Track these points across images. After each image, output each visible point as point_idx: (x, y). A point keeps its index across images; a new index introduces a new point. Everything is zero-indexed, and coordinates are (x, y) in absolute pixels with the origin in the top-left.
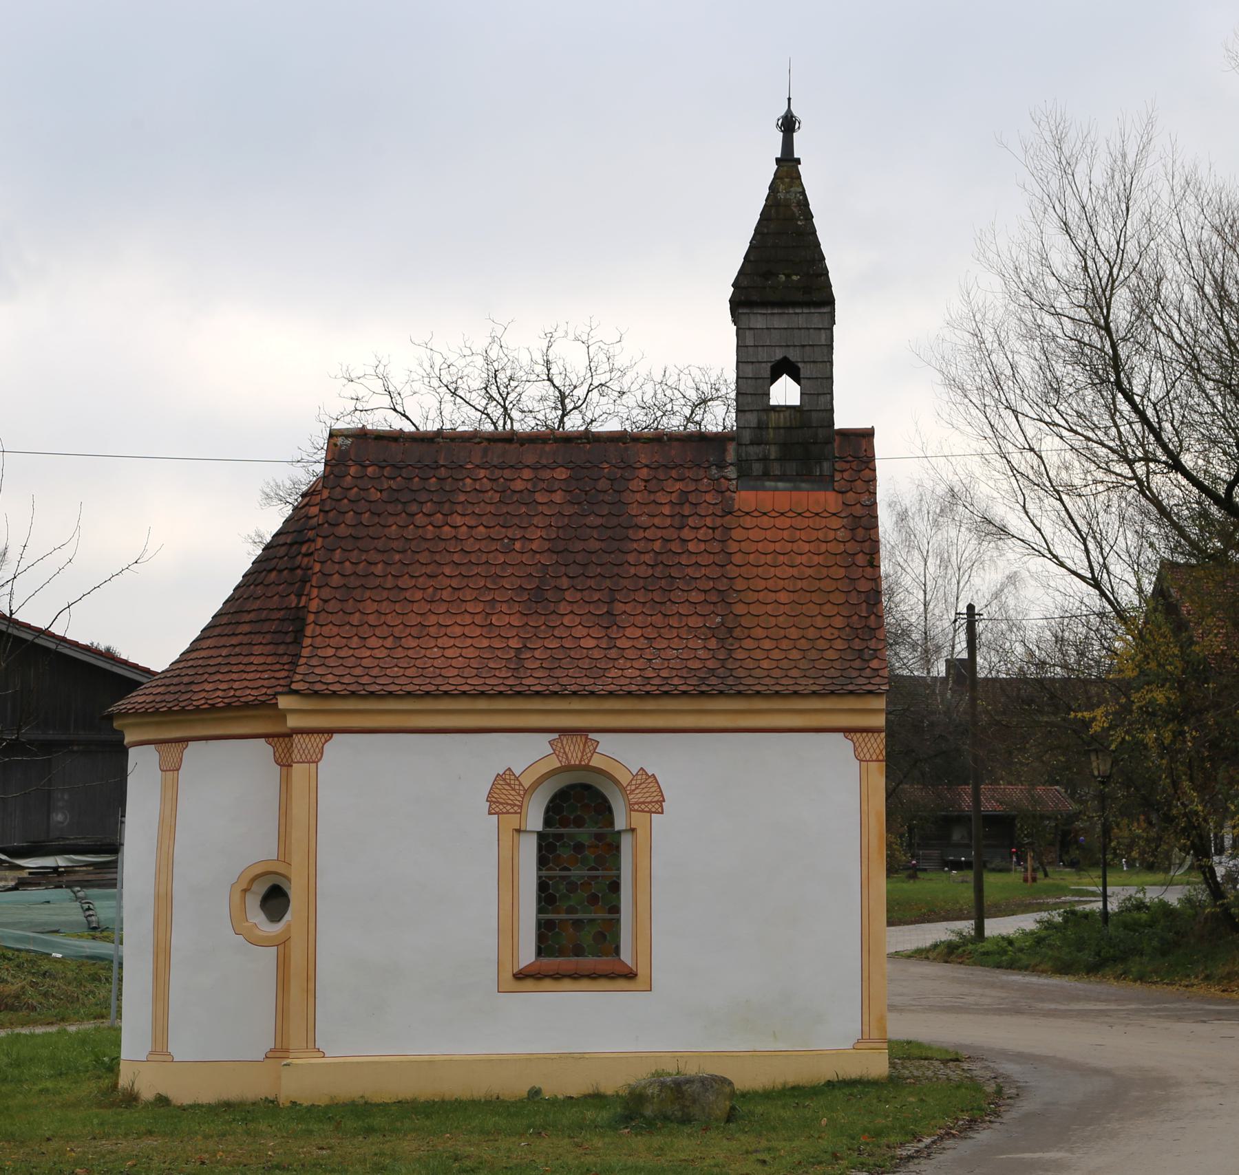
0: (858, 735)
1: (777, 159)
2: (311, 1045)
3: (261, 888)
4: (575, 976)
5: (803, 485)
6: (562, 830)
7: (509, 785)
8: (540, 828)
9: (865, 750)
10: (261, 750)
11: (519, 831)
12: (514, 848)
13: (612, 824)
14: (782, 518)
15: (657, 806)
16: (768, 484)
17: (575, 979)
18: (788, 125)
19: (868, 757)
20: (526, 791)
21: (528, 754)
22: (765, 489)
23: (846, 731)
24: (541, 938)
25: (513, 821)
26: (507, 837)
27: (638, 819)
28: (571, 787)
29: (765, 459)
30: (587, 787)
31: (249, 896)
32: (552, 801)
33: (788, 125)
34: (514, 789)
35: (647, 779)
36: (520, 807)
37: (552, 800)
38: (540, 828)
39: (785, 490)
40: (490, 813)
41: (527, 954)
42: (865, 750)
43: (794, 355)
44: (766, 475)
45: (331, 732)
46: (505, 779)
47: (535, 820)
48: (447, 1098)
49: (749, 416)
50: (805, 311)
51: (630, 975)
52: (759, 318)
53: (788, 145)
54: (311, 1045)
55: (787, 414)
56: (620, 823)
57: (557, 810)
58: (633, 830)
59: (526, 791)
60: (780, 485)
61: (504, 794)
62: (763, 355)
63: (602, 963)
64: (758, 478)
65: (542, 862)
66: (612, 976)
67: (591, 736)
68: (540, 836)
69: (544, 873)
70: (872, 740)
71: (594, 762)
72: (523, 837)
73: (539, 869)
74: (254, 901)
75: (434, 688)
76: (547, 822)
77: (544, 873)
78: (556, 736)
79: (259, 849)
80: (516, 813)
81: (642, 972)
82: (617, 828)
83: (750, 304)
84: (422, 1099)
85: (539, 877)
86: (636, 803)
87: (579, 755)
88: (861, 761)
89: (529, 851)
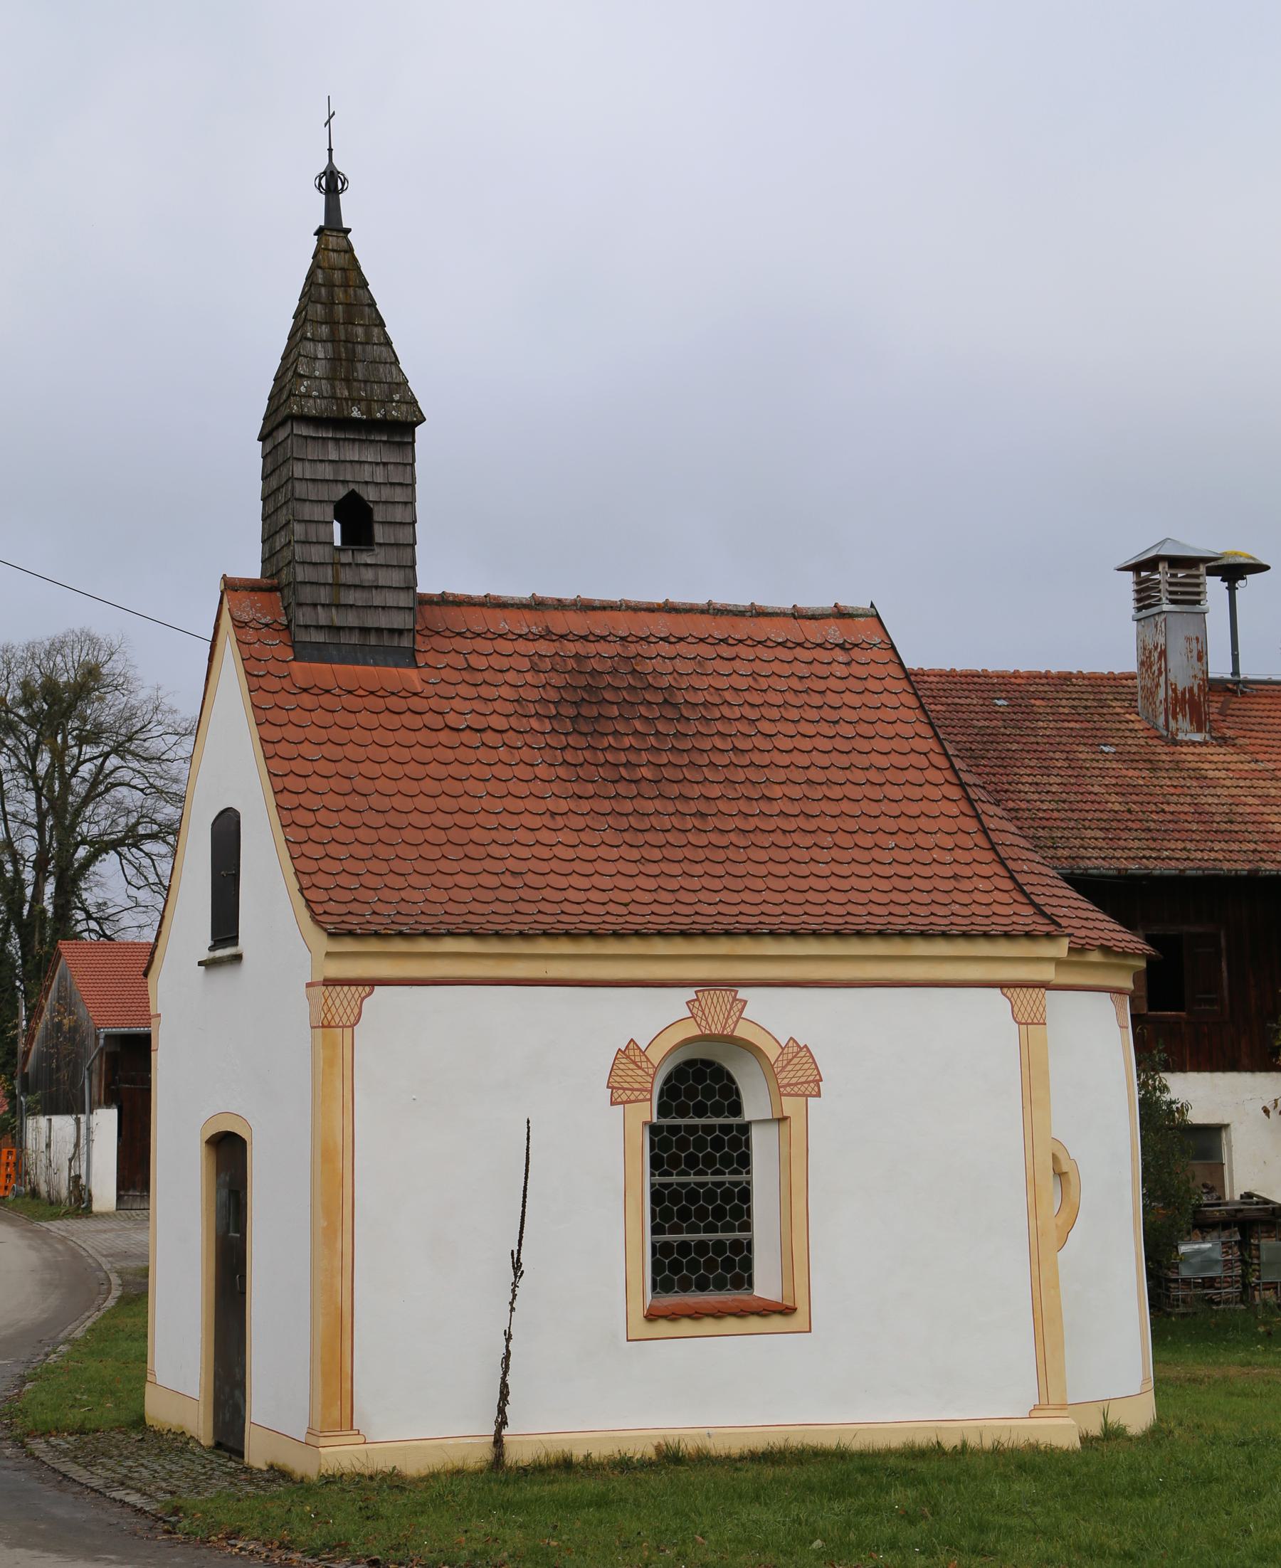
2: (346, 1425)
4: (696, 1315)
13: (736, 1109)
18: (332, 184)
21: (654, 1020)
23: (1002, 985)
33: (332, 184)
34: (640, 1068)
35: (799, 1052)
40: (612, 1104)
45: (373, 983)
47: (647, 1111)
48: (973, 1441)
53: (333, 210)
54: (346, 1425)
66: (741, 1313)
67: (743, 993)
69: (743, 1177)
70: (1022, 996)
71: (742, 1031)
76: (663, 1110)
78: (690, 993)
82: (749, 1114)
84: (988, 1444)
88: (1020, 1023)
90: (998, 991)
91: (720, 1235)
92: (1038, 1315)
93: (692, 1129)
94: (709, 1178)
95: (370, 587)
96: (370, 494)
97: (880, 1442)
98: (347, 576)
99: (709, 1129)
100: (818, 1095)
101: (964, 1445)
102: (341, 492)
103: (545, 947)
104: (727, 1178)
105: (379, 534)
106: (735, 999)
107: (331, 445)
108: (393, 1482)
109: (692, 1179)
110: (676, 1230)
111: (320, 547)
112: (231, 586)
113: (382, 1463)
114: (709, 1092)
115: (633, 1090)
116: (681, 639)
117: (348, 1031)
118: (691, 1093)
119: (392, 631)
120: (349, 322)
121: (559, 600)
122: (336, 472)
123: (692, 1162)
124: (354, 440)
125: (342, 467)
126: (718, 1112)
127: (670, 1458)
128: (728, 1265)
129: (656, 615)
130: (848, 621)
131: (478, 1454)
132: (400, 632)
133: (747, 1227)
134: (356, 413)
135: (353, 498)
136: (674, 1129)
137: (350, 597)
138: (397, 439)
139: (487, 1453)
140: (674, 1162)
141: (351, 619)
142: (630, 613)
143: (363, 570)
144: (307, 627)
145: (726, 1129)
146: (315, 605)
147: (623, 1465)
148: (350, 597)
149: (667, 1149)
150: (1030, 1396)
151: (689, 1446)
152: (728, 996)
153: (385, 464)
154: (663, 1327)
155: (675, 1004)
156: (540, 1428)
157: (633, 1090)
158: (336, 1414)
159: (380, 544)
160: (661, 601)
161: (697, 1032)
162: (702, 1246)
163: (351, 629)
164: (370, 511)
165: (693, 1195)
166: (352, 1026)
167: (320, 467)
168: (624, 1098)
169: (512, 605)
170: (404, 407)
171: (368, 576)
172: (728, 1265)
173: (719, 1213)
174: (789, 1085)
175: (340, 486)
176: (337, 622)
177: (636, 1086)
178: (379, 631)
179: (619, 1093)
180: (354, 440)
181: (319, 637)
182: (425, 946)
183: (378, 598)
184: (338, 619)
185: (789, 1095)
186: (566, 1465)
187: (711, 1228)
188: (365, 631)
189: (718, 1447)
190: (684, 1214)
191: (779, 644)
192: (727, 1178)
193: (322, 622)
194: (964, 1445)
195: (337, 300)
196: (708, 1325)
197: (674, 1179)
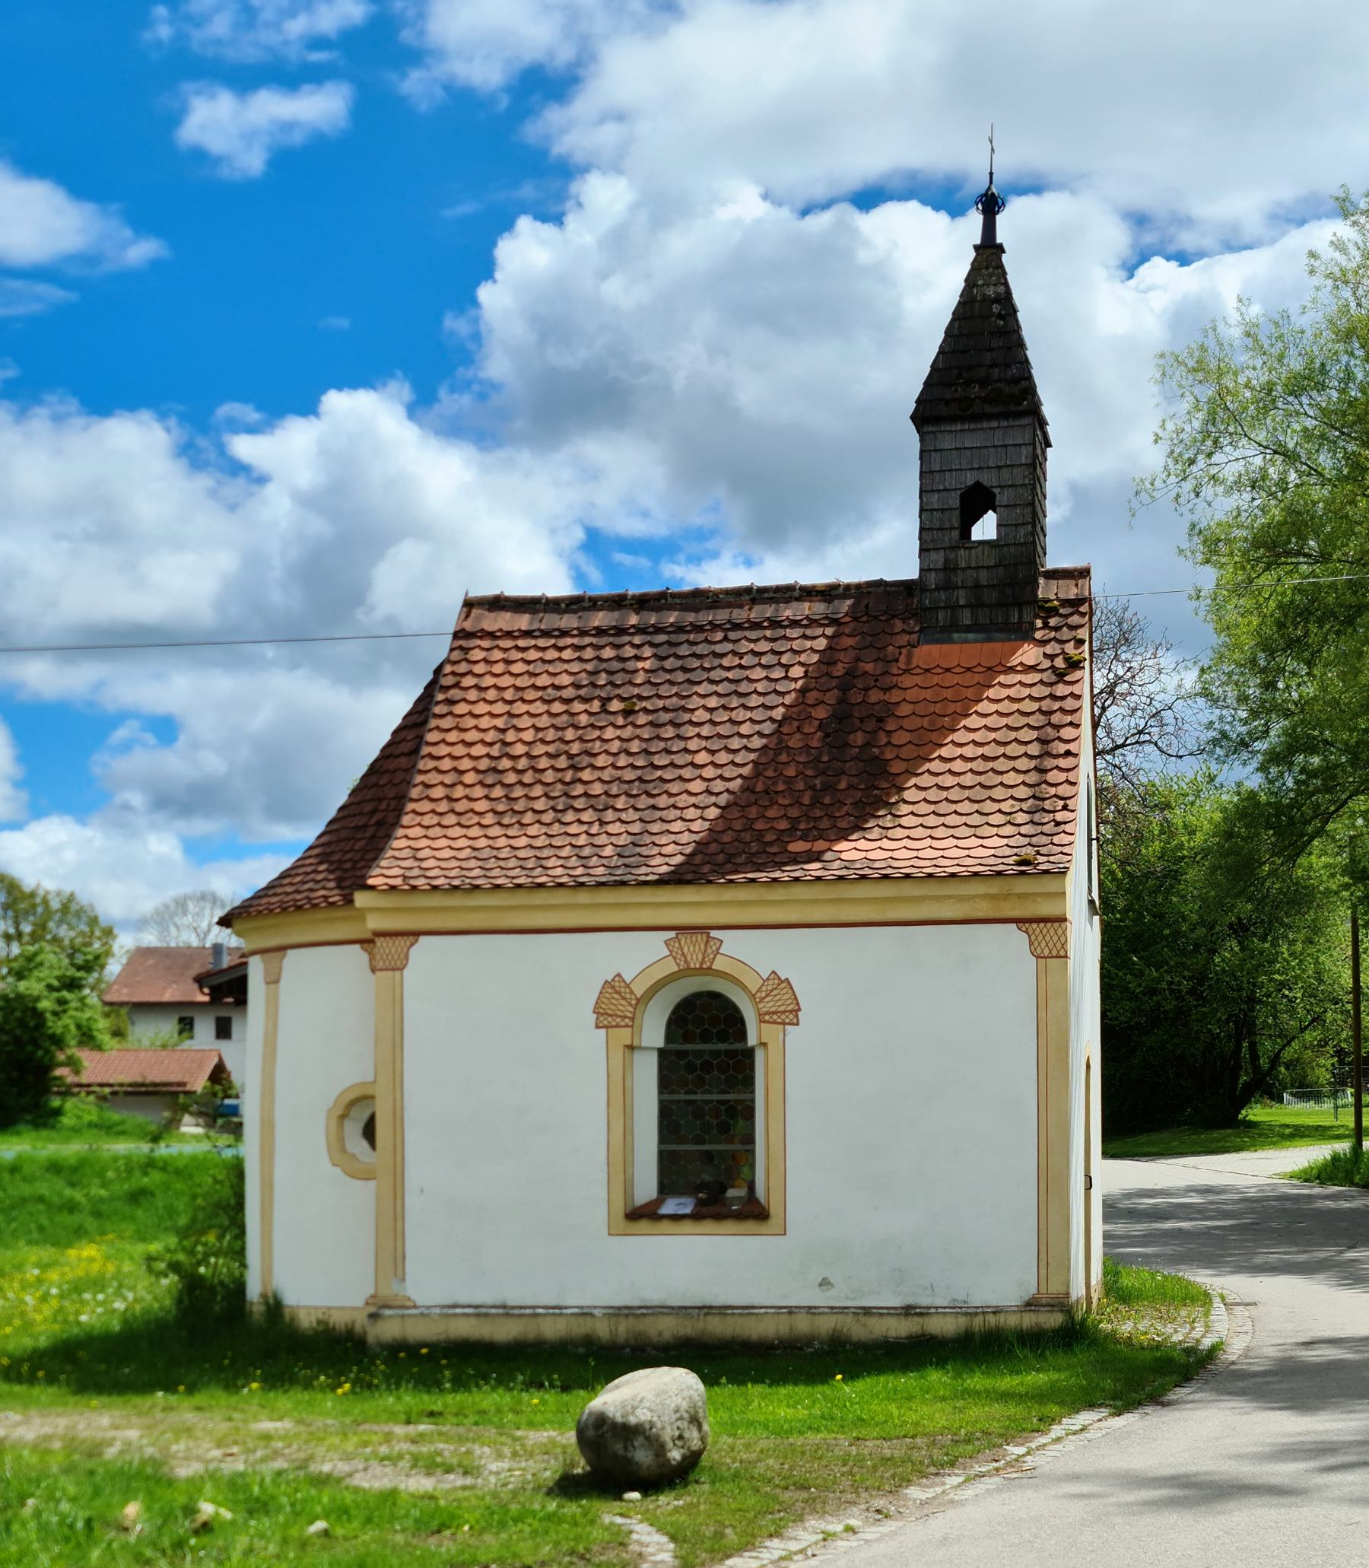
0: (1035, 926)
1: (976, 247)
5: (998, 635)
7: (618, 993)
8: (661, 1044)
9: (1043, 944)
10: (1013, 938)
11: (631, 1048)
12: (627, 1068)
13: (742, 1035)
14: (969, 674)
15: (791, 1014)
16: (956, 636)
19: (1046, 952)
20: (638, 1000)
21: (640, 957)
22: (950, 641)
25: (624, 1036)
26: (618, 1055)
27: (770, 1032)
29: (954, 608)
31: (347, 1124)
32: (674, 1012)
34: (624, 998)
35: (779, 983)
36: (633, 1019)
38: (661, 1044)
39: (976, 641)
40: (597, 1027)
41: (647, 1188)
42: (1043, 944)
43: (988, 479)
44: (954, 626)
46: (614, 987)
47: (654, 1033)
49: (933, 555)
50: (1004, 423)
52: (948, 437)
53: (989, 228)
55: (980, 549)
56: (752, 1040)
58: (764, 1045)
59: (638, 1000)
60: (971, 636)
61: (614, 1006)
62: (951, 481)
64: (943, 629)
65: (664, 1084)
67: (714, 933)
68: (661, 1052)
69: (667, 1097)
72: (638, 1056)
73: (661, 1092)
75: (506, 881)
76: (669, 1038)
77: (667, 1097)
78: (672, 934)
79: (354, 1069)
80: (627, 1026)
81: (774, 1209)
83: (937, 420)
86: (768, 1013)
87: (700, 956)
88: (1038, 957)
117: (397, 973)
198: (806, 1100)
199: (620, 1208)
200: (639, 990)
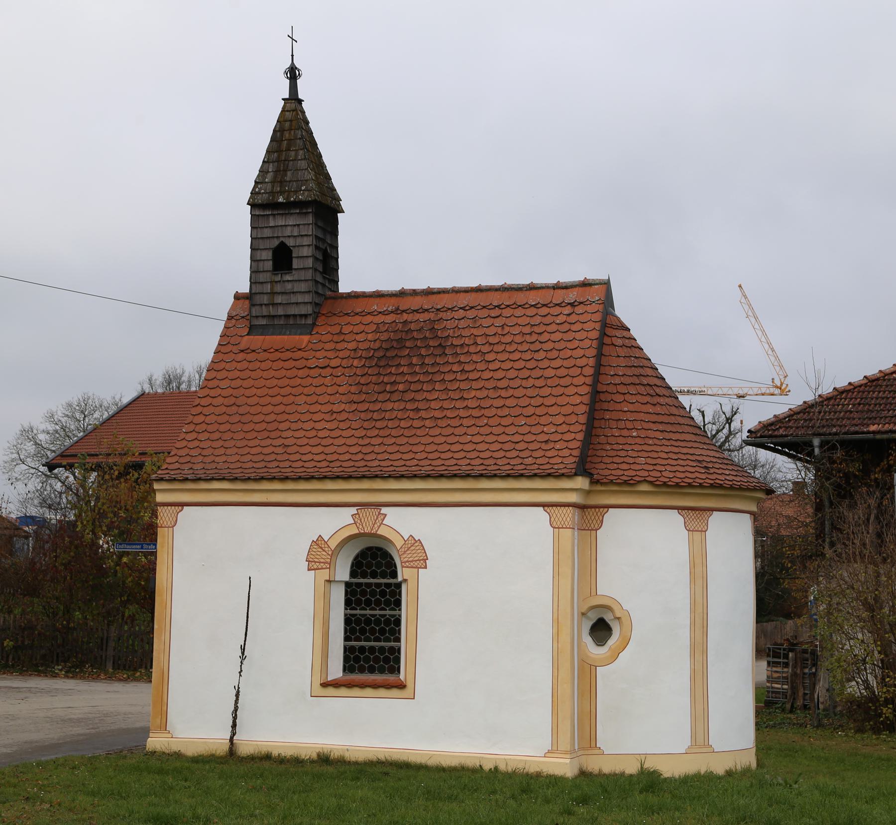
3: (594, 617)
4: (375, 686)
6: (372, 581)
11: (329, 581)
13: (394, 575)
15: (422, 562)
17: (349, 687)
18: (293, 74)
21: (333, 523)
24: (346, 659)
25: (325, 574)
28: (369, 549)
30: (380, 549)
33: (293, 74)
35: (415, 544)
37: (356, 558)
41: (336, 670)
45: (183, 505)
47: (343, 573)
48: (502, 767)
51: (402, 686)
53: (293, 88)
57: (357, 568)
61: (319, 555)
63: (390, 678)
66: (388, 686)
67: (384, 510)
68: (348, 585)
69: (397, 612)
71: (380, 532)
72: (333, 586)
74: (587, 625)
76: (353, 574)
78: (353, 510)
81: (409, 684)
83: (273, 206)
85: (346, 615)
88: (554, 528)
89: (338, 595)
90: (541, 508)
91: (382, 644)
92: (555, 699)
93: (369, 585)
94: (377, 612)
95: (290, 293)
96: (290, 242)
97: (446, 762)
98: (278, 288)
99: (378, 585)
100: (426, 567)
101: (496, 768)
102: (276, 243)
103: (266, 485)
104: (388, 612)
105: (295, 266)
106: (379, 513)
107: (271, 218)
108: (178, 755)
109: (368, 612)
110: (358, 639)
111: (265, 274)
112: (238, 297)
113: (175, 748)
114: (379, 565)
115: (320, 562)
116: (472, 308)
117: (171, 529)
118: (369, 565)
119: (301, 316)
120: (288, 149)
121: (414, 290)
122: (273, 233)
123: (368, 603)
124: (282, 214)
125: (276, 229)
126: (384, 576)
127: (324, 759)
128: (387, 660)
129: (469, 294)
130: (588, 288)
131: (222, 748)
132: (306, 316)
133: (398, 640)
134: (281, 200)
135: (282, 244)
136: (359, 585)
137: (279, 299)
138: (304, 211)
139: (226, 747)
140: (358, 603)
141: (280, 311)
142: (454, 294)
143: (286, 284)
144: (257, 317)
145: (388, 585)
146: (261, 305)
147: (297, 761)
148: (279, 299)
149: (354, 595)
150: (546, 743)
151: (335, 755)
152: (377, 511)
153: (298, 225)
154: (331, 691)
155: (345, 516)
156: (258, 736)
157: (320, 562)
158: (159, 721)
159: (296, 269)
160: (398, 288)
161: (356, 531)
162: (372, 649)
163: (280, 316)
164: (291, 251)
165: (368, 621)
166: (173, 527)
167: (266, 230)
168: (315, 567)
169: (387, 295)
170: (306, 193)
171: (289, 286)
172: (387, 660)
173: (382, 632)
174: (408, 561)
175: (275, 240)
176: (272, 313)
177: (322, 560)
178: (295, 316)
179: (312, 564)
180: (282, 214)
181: (263, 322)
182: (203, 485)
183: (294, 299)
184: (272, 311)
185: (407, 567)
186: (268, 757)
187: (377, 640)
188: (287, 316)
189: (351, 756)
190: (363, 631)
191: (532, 306)
192: (388, 612)
193: (265, 313)
194: (496, 768)
195: (292, 137)
196: (369, 692)
197: (358, 612)
198: (302, 616)
199: (317, 682)
200: (333, 544)
